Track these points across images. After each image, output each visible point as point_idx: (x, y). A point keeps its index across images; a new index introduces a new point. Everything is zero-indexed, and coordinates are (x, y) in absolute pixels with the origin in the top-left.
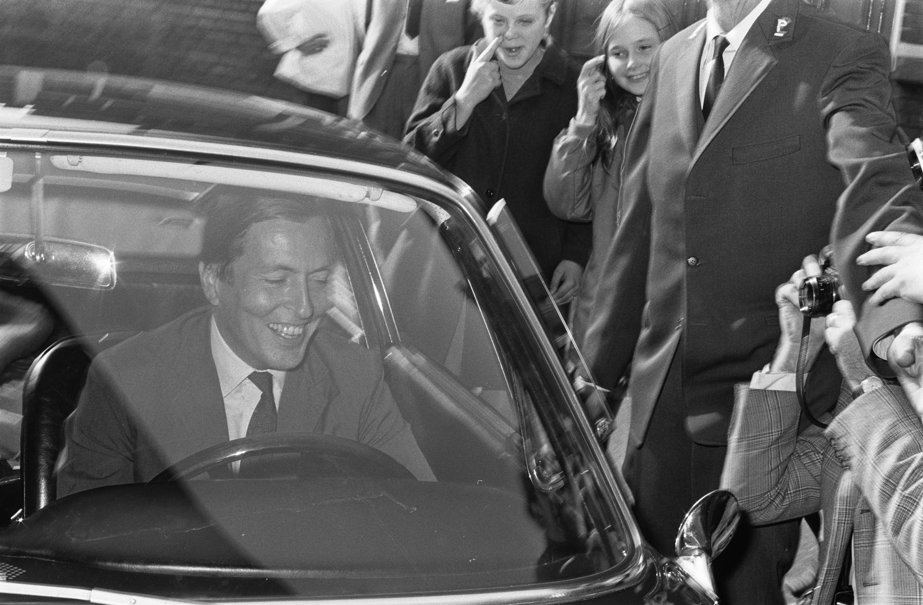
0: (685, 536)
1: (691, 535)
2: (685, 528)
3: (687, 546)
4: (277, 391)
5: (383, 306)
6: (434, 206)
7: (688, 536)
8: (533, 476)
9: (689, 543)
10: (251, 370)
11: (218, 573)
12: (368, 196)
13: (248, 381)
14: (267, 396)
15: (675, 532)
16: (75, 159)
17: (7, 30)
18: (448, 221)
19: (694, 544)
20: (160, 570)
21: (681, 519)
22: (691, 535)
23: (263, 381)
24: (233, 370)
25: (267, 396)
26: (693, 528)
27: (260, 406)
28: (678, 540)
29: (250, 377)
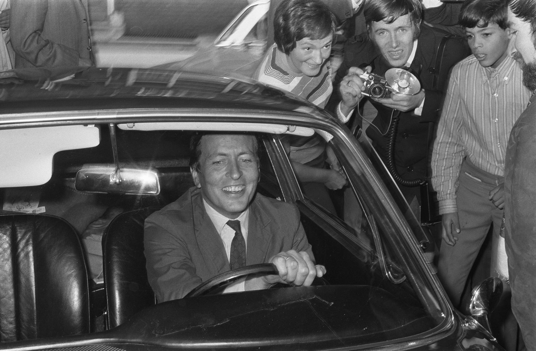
0: (475, 303)
1: (478, 302)
2: (475, 298)
3: (477, 309)
4: (244, 231)
5: (426, 294)
6: (324, 132)
7: (476, 303)
8: (389, 275)
9: (477, 307)
10: (227, 219)
11: (230, 346)
12: (288, 130)
13: (227, 226)
14: (238, 234)
15: (470, 302)
16: (132, 124)
17: (3, 75)
18: (332, 140)
19: (480, 307)
20: (201, 346)
21: (471, 295)
22: (478, 302)
23: (235, 225)
24: (219, 220)
25: (238, 234)
26: (478, 299)
27: (235, 239)
28: (471, 305)
29: (227, 223)
